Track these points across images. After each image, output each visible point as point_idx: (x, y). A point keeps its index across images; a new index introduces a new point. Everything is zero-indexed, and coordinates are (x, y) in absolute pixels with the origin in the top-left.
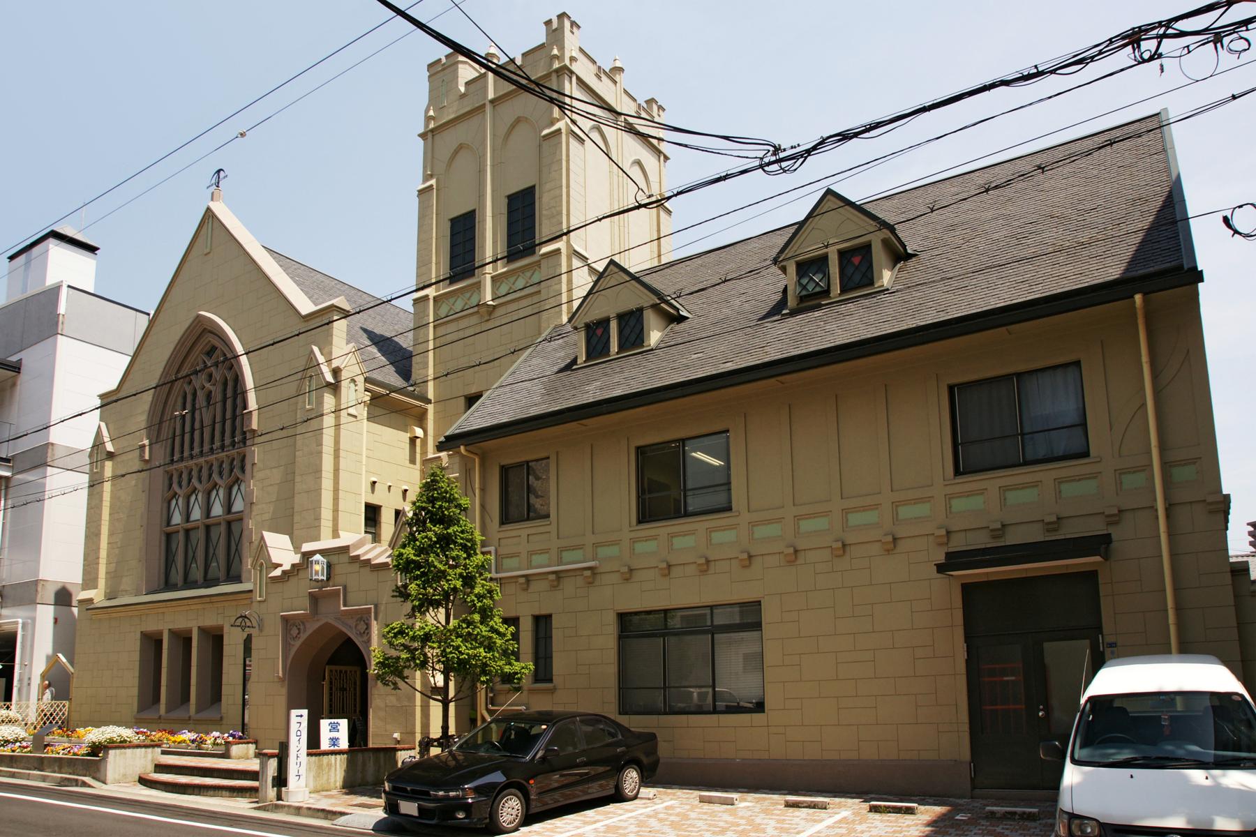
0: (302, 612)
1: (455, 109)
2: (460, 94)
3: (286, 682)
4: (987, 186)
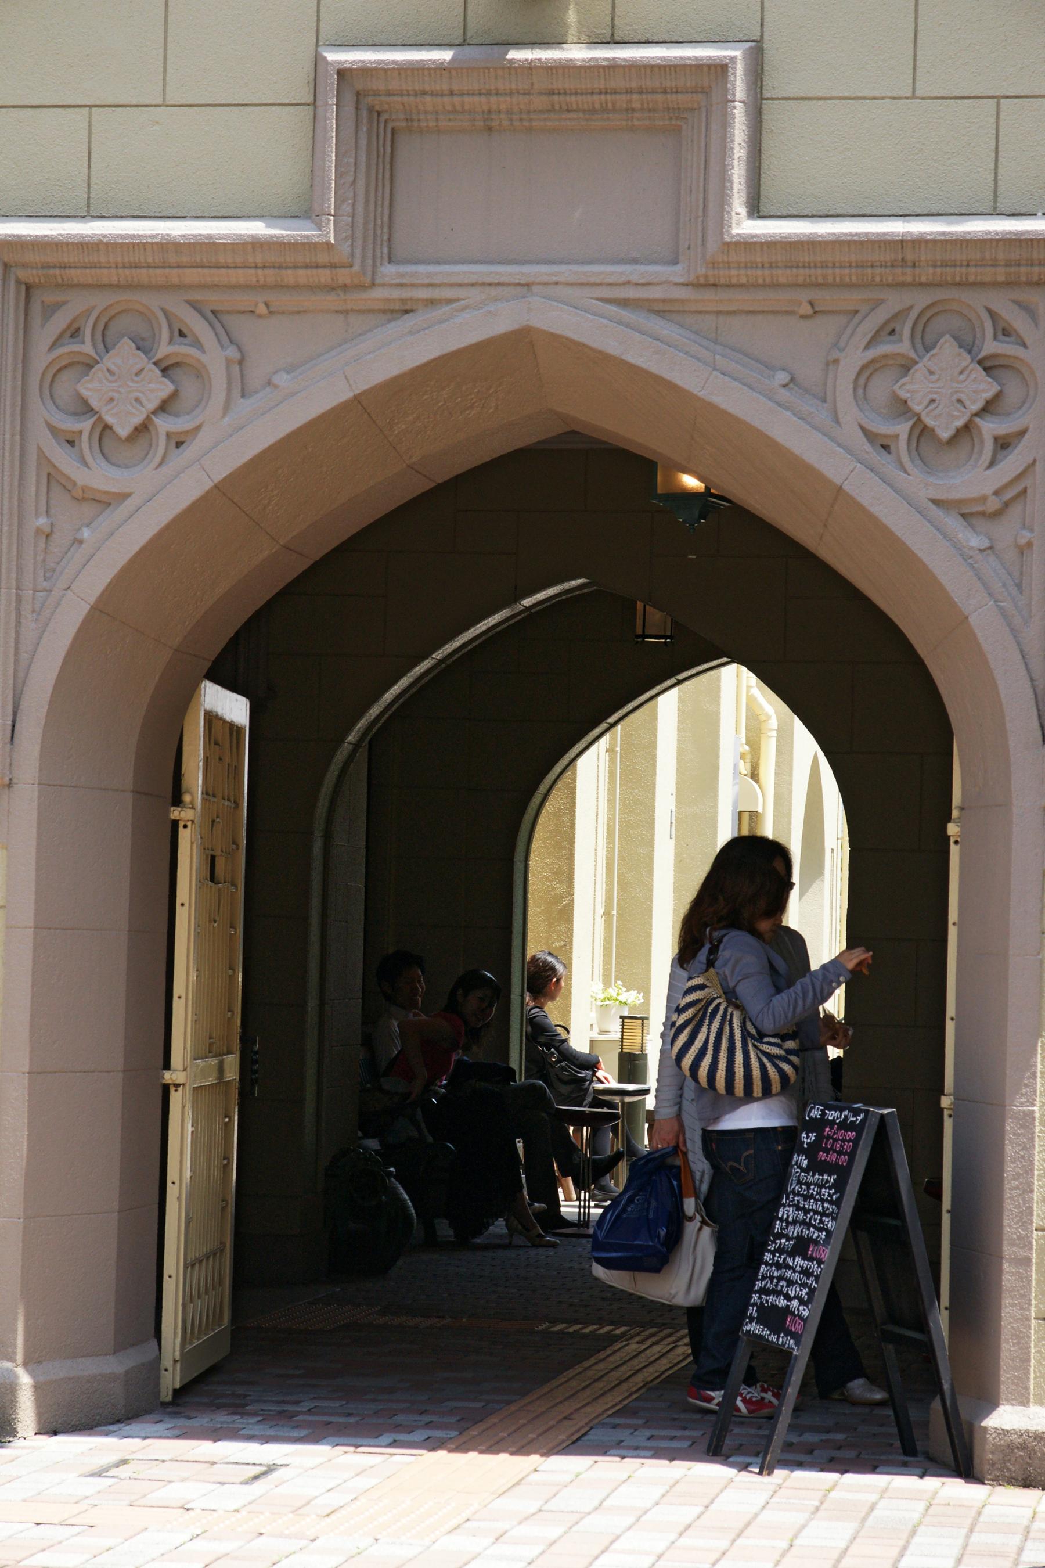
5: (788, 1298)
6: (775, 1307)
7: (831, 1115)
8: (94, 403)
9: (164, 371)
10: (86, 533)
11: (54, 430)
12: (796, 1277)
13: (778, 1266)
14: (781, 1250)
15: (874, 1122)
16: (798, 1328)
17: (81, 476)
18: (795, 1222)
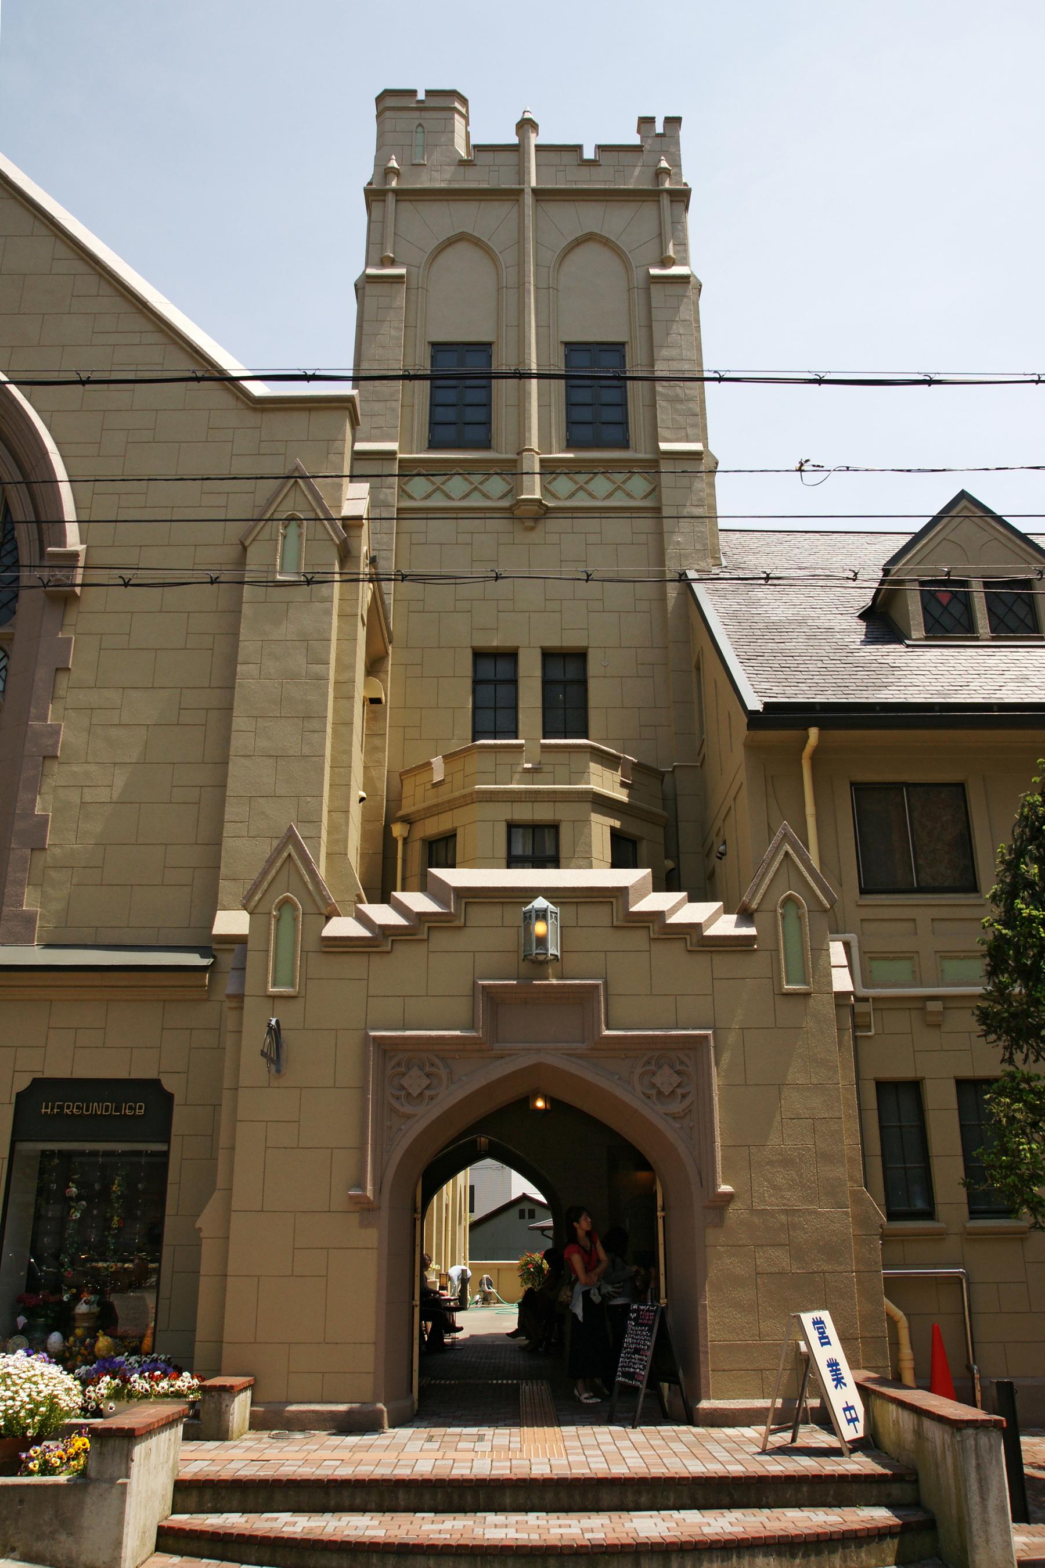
0: (458, 1033)
1: (448, 176)
2: (459, 158)
3: (385, 1214)
4: (309, 576)
5: (634, 1368)
6: (629, 1372)
7: (642, 1307)
8: (405, 1086)
9: (427, 1076)
10: (403, 1127)
11: (393, 1095)
12: (636, 1361)
13: (628, 1358)
14: (628, 1353)
15: (660, 1309)
16: (641, 1378)
17: (402, 1110)
18: (632, 1343)
